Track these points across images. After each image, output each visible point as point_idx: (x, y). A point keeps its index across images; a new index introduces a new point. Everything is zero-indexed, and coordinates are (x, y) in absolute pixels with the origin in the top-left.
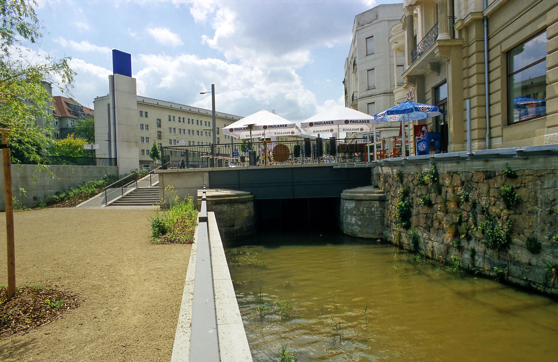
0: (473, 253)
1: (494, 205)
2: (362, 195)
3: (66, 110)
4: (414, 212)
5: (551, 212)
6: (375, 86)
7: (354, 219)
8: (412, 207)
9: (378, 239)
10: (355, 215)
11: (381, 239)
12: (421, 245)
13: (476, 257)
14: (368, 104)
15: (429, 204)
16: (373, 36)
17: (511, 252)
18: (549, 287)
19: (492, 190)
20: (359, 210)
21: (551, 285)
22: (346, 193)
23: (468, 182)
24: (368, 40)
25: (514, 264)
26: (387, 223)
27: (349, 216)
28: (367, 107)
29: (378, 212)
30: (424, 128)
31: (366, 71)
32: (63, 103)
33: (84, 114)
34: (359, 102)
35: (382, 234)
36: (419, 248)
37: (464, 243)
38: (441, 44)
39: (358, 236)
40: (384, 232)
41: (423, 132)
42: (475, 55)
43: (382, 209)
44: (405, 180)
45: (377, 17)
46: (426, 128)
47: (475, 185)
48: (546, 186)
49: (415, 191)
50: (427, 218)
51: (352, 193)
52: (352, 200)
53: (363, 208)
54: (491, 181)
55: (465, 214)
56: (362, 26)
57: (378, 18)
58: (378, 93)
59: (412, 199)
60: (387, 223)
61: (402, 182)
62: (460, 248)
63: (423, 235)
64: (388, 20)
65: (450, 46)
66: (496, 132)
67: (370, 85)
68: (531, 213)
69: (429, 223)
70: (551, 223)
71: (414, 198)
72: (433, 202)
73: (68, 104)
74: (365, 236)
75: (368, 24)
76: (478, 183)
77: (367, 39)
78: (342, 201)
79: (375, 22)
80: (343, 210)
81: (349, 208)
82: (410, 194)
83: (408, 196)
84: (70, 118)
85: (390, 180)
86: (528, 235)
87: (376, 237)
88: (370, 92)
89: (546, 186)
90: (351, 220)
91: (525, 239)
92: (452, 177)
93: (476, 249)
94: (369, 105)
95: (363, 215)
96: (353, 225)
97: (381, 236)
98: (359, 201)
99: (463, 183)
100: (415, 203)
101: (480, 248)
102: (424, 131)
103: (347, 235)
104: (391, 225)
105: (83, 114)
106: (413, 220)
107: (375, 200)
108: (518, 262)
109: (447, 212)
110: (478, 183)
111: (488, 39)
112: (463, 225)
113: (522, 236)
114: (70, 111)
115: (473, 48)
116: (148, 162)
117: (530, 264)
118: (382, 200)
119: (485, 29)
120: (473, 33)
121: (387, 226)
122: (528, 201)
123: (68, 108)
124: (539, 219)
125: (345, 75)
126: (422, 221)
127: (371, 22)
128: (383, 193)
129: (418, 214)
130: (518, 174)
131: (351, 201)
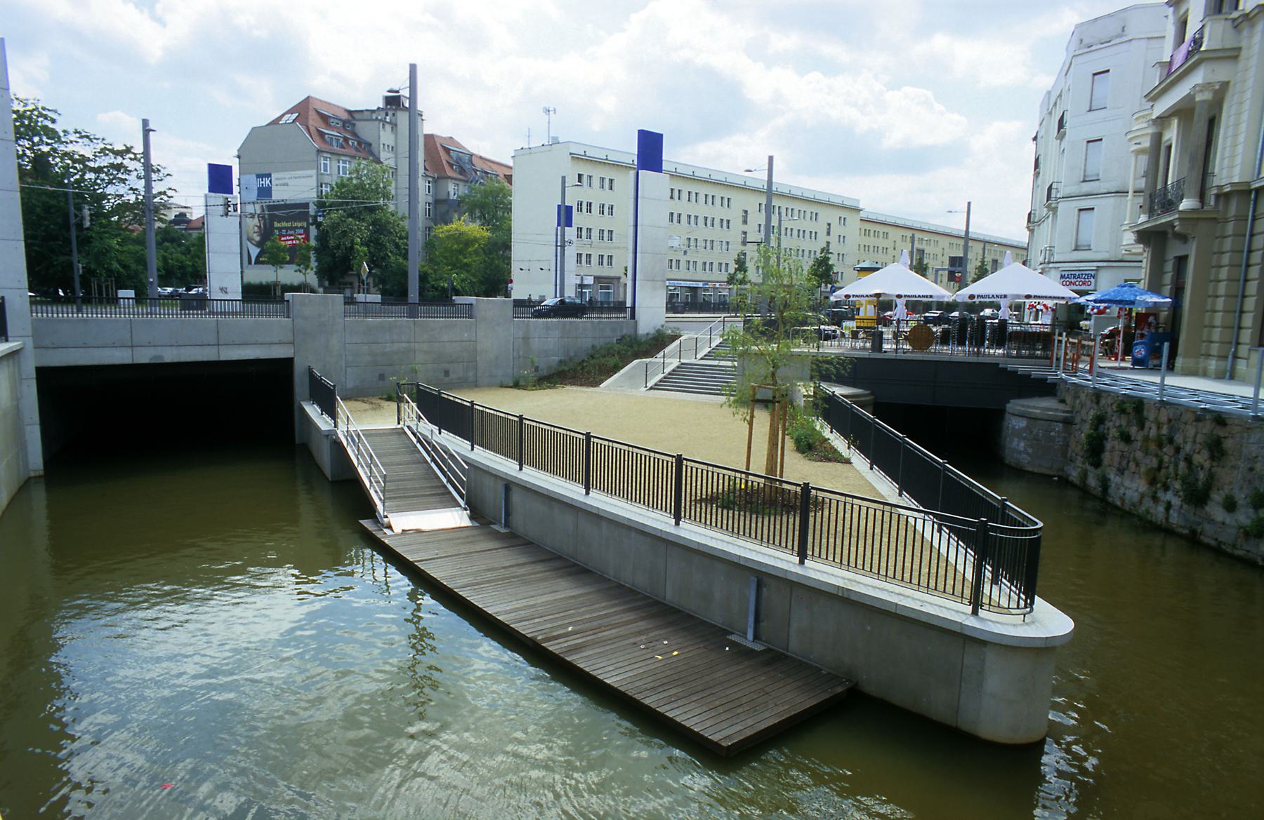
0: (1169, 506)
1: (1199, 453)
2: (1039, 411)
3: (444, 162)
4: (1108, 445)
5: (1251, 469)
6: (1098, 175)
7: (1022, 444)
8: (1107, 439)
9: (1055, 476)
10: (1025, 438)
11: (1059, 477)
12: (1111, 491)
13: (1171, 512)
14: (1080, 210)
15: (1126, 438)
16: (1108, 71)
17: (1207, 509)
18: (1237, 549)
19: (1199, 436)
20: (1031, 432)
21: (1239, 547)
22: (1015, 405)
23: (1175, 420)
24: (1096, 77)
25: (1209, 523)
26: (1071, 457)
27: (1016, 439)
28: (1085, 149)
29: (1060, 439)
30: (1151, 319)
31: (1085, 143)
32: (440, 149)
33: (476, 171)
34: (1060, 204)
35: (1062, 470)
36: (1108, 494)
37: (1160, 494)
38: (1184, 216)
39: (1027, 469)
40: (1065, 469)
41: (1150, 325)
42: (1230, 239)
43: (1066, 435)
44: (1103, 401)
45: (1123, 31)
46: (1156, 319)
47: (1182, 426)
48: (1251, 441)
49: (1113, 418)
50: (1122, 457)
51: (1023, 406)
52: (1022, 416)
53: (1039, 430)
54: (1200, 424)
55: (1166, 459)
56: (1089, 47)
57: (1125, 33)
58: (1105, 191)
59: (1108, 429)
60: (1071, 457)
61: (1098, 403)
62: (1155, 498)
63: (1114, 478)
64: (1148, 38)
65: (1198, 219)
66: (1243, 351)
67: (1088, 173)
68: (1233, 467)
69: (1124, 463)
70: (1249, 481)
71: (1111, 428)
72: (1133, 439)
73: (447, 151)
74: (1036, 470)
75: (1102, 44)
76: (1186, 424)
77: (1095, 74)
78: (1007, 416)
79: (1118, 40)
80: (1008, 428)
81: (1017, 427)
82: (1106, 422)
83: (1103, 423)
84: (452, 178)
85: (1083, 396)
86: (1226, 491)
87: (1052, 473)
88: (1086, 188)
89: (1251, 441)
90: (1018, 445)
91: (1224, 496)
92: (1159, 410)
93: (1173, 503)
94: (1082, 213)
95: (1037, 440)
96: (1020, 452)
97: (1060, 473)
98: (1032, 419)
99: (1170, 421)
100: (1111, 435)
101: (1176, 502)
102: (1151, 323)
103: (1010, 467)
104: (1076, 459)
105: (473, 169)
106: (1106, 457)
107: (1057, 422)
108: (1213, 520)
109: (1147, 453)
110: (1186, 424)
111: (1254, 219)
112: (1163, 471)
113: (1221, 491)
114: (451, 165)
115: (1230, 229)
116: (609, 280)
117: (1223, 523)
118: (1068, 422)
119: (1251, 206)
120: (1233, 209)
121: (1071, 460)
122: (1232, 455)
123: (448, 158)
124: (1240, 475)
125: (1041, 124)
126: (1117, 459)
127: (1109, 41)
128: (1071, 412)
129: (1112, 451)
130: (1229, 422)
131: (1020, 419)
